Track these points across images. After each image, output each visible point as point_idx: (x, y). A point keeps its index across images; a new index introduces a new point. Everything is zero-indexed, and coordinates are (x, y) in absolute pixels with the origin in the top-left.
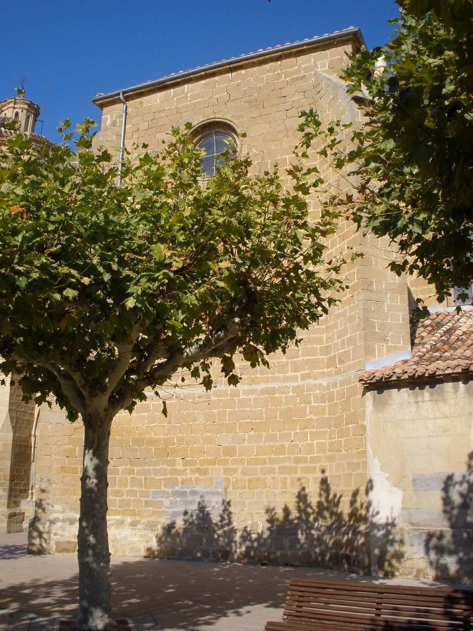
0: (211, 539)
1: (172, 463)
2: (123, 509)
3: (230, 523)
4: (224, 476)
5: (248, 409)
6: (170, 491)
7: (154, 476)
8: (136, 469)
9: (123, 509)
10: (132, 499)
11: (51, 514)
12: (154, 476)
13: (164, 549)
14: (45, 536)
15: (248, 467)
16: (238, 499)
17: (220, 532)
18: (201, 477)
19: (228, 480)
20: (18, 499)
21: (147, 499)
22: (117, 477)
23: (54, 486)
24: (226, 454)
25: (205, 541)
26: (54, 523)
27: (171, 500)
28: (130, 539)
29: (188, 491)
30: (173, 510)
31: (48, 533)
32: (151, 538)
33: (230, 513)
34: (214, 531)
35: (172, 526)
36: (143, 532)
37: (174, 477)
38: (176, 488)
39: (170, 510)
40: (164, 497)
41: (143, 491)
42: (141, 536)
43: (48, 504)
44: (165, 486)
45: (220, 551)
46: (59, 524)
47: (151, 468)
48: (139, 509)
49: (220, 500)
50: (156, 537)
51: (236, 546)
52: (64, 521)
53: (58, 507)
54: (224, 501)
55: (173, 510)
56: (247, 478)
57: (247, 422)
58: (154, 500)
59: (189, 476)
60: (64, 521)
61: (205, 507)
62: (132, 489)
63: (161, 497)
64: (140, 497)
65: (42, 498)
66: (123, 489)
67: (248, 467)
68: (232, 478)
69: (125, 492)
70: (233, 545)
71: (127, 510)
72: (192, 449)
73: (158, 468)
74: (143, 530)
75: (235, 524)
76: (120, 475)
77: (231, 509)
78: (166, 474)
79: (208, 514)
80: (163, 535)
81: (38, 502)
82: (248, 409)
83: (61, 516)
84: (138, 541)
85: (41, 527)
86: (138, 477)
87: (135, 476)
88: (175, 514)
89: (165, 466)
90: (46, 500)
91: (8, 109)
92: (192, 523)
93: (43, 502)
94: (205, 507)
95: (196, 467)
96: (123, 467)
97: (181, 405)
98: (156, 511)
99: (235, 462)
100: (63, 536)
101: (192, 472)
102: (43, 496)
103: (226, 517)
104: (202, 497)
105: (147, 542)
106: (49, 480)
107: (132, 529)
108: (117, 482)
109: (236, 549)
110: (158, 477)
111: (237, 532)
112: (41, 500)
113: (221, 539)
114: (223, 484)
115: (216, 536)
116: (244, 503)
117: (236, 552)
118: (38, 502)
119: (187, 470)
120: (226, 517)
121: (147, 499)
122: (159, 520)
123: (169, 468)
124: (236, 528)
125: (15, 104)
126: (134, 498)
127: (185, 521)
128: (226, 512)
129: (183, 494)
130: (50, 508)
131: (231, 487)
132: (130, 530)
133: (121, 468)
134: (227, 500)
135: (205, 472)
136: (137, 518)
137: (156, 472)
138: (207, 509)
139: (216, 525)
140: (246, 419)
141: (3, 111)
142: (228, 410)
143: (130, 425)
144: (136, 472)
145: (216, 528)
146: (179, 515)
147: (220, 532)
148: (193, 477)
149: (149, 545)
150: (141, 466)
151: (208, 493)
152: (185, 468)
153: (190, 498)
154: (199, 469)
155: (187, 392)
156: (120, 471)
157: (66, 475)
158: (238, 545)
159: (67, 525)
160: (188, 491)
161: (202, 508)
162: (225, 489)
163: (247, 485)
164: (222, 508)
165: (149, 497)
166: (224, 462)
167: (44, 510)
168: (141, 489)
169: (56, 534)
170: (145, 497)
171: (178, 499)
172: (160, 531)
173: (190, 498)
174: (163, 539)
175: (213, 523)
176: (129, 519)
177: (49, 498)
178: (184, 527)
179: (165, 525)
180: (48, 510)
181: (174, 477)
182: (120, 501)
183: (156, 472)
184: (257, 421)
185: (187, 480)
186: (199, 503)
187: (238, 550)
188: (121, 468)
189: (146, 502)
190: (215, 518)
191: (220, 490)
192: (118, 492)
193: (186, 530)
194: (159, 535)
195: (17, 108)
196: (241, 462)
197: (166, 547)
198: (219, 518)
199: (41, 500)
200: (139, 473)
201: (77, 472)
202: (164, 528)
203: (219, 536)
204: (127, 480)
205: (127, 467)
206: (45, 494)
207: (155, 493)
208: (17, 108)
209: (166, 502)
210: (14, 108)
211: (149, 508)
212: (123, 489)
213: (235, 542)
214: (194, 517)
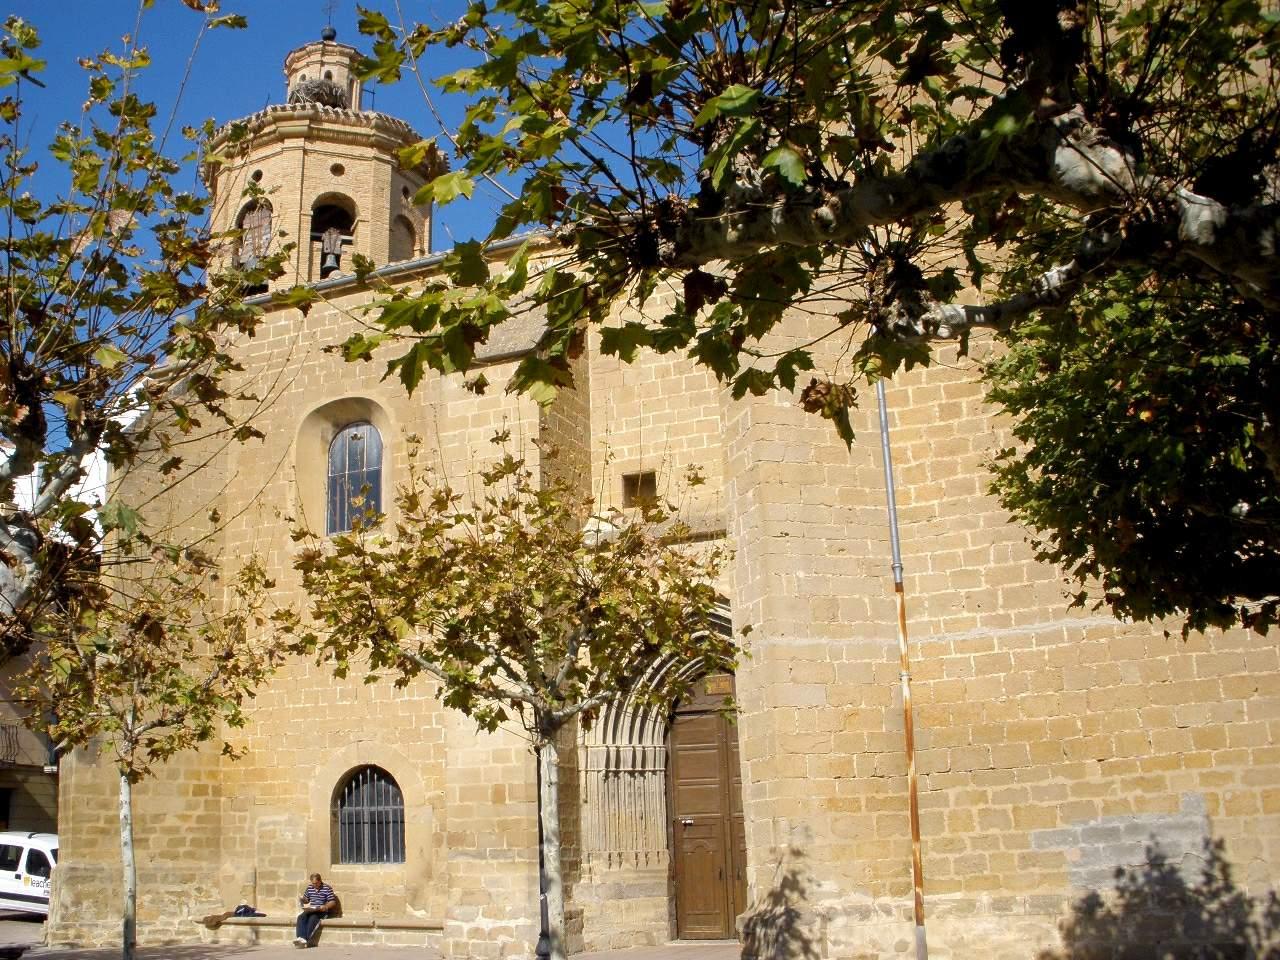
0: (1193, 923)
1: (1076, 771)
2: (968, 877)
3: (1228, 888)
4: (1202, 790)
5: (1240, 650)
6: (1079, 829)
7: (1036, 803)
8: (990, 790)
9: (968, 877)
10: (987, 854)
11: (818, 900)
12: (1036, 803)
13: (1083, 952)
14: (816, 947)
15: (1257, 767)
16: (1244, 835)
17: (1214, 906)
18: (1148, 796)
19: (1215, 798)
20: (569, 883)
21: (1024, 851)
22: (947, 811)
23: (818, 841)
24: (1200, 745)
25: (1179, 928)
26: (830, 920)
27: (1082, 849)
28: (995, 937)
29: (1122, 826)
30: (1090, 867)
31: (820, 940)
32: (1048, 932)
33: (1225, 868)
34: (1200, 907)
35: (1091, 904)
36: (1028, 921)
37: (1084, 799)
38: (1092, 823)
39: (1080, 870)
40: (1064, 842)
41: (1012, 836)
42: (1021, 930)
43: (810, 881)
44: (1065, 820)
45: (1219, 947)
46: (840, 921)
47: (1028, 785)
48: (1007, 873)
49: (1199, 840)
50: (1061, 927)
51: (1258, 934)
52: (847, 913)
53: (829, 886)
54: (1207, 843)
55: (1090, 867)
56: (1257, 790)
57: (1243, 677)
58: (1042, 851)
59: (1120, 795)
60: (847, 913)
61: (1164, 858)
62: (985, 833)
63: (1058, 844)
64: (1007, 847)
65: (797, 869)
66: (964, 835)
67: (1257, 767)
68: (1223, 792)
69: (968, 842)
70: (1250, 931)
71: (976, 878)
72: (1119, 739)
73: (1044, 783)
74: (1027, 918)
75: (1244, 886)
76: (952, 807)
77: (1228, 856)
78: (1065, 796)
79: (1173, 871)
80: (1078, 922)
81: (790, 877)
82: (1240, 650)
83: (837, 904)
84: (1016, 941)
85: (804, 930)
86: (997, 807)
87: (990, 805)
88: (1097, 877)
89: (1060, 780)
90: (804, 871)
91: (308, 65)
92: (1137, 893)
93: (799, 878)
94: (1164, 858)
95: (1135, 775)
96: (959, 789)
97: (1082, 652)
98: (1049, 874)
99: (1222, 760)
100: (851, 944)
101: (1126, 785)
102: (798, 864)
103: (1217, 873)
104: (1152, 836)
105: (1039, 939)
106: (807, 829)
107: (1000, 916)
108: (946, 823)
109: (1259, 939)
110: (1045, 804)
111: (1257, 903)
112: (794, 874)
113: (1218, 920)
114: (1202, 804)
115: (1205, 916)
116: (1258, 842)
117: (1259, 946)
118: (790, 877)
119: (1113, 782)
120: (1217, 873)
121: (1024, 851)
122: (1060, 891)
123: (1069, 782)
124: (1248, 895)
125: (323, 55)
126: (991, 852)
127: (1121, 891)
128: (1217, 865)
129: (1112, 833)
130: (815, 888)
131: (1222, 810)
132: (996, 919)
133: (952, 793)
134: (1216, 838)
135: (1157, 784)
136: (1006, 893)
137: (1040, 793)
138: (1167, 862)
139: (1198, 891)
140: (1237, 670)
141: (296, 70)
142: (1194, 655)
143: (964, 700)
144: (990, 797)
145: (1201, 899)
146: (1105, 878)
147: (1214, 906)
148: (1130, 796)
149: (1045, 946)
150: (1003, 784)
151: (1170, 827)
152: (1109, 779)
153: (1128, 841)
154: (1142, 778)
155: (1094, 623)
156: (952, 798)
157: (838, 815)
158: (1263, 933)
159: (855, 922)
160: (1122, 826)
161: (1155, 860)
162: (1207, 817)
163: (1259, 804)
164: (1206, 856)
165: (1028, 847)
166: (1201, 761)
167: (802, 893)
168: (1007, 832)
169: (836, 943)
170: (1017, 848)
171: (1101, 845)
172: (1068, 914)
173: (1128, 841)
174: (1078, 931)
175: (1190, 890)
176: (985, 898)
177: (810, 868)
178: (1121, 901)
179: (1077, 903)
180: (812, 893)
181: (1084, 799)
182: (956, 861)
183: (1040, 793)
184: (1265, 673)
185: (1116, 803)
186: (1149, 850)
187: (1266, 944)
188: (951, 793)
189: (1023, 857)
190: (1193, 880)
191: (1198, 819)
192: (951, 841)
193: (1129, 908)
194: (1066, 924)
195: (328, 63)
196: (1240, 758)
197: (1087, 948)
198: (1201, 879)
199: (794, 874)
200: (997, 798)
201: (860, 809)
202: (1077, 909)
203: (1213, 915)
204: (970, 817)
205: (968, 789)
206: (801, 859)
207: (1039, 837)
208: (328, 63)
209: (1072, 853)
210: (323, 64)
211: (1032, 869)
212: (964, 835)
213: (1255, 926)
214: (1141, 880)
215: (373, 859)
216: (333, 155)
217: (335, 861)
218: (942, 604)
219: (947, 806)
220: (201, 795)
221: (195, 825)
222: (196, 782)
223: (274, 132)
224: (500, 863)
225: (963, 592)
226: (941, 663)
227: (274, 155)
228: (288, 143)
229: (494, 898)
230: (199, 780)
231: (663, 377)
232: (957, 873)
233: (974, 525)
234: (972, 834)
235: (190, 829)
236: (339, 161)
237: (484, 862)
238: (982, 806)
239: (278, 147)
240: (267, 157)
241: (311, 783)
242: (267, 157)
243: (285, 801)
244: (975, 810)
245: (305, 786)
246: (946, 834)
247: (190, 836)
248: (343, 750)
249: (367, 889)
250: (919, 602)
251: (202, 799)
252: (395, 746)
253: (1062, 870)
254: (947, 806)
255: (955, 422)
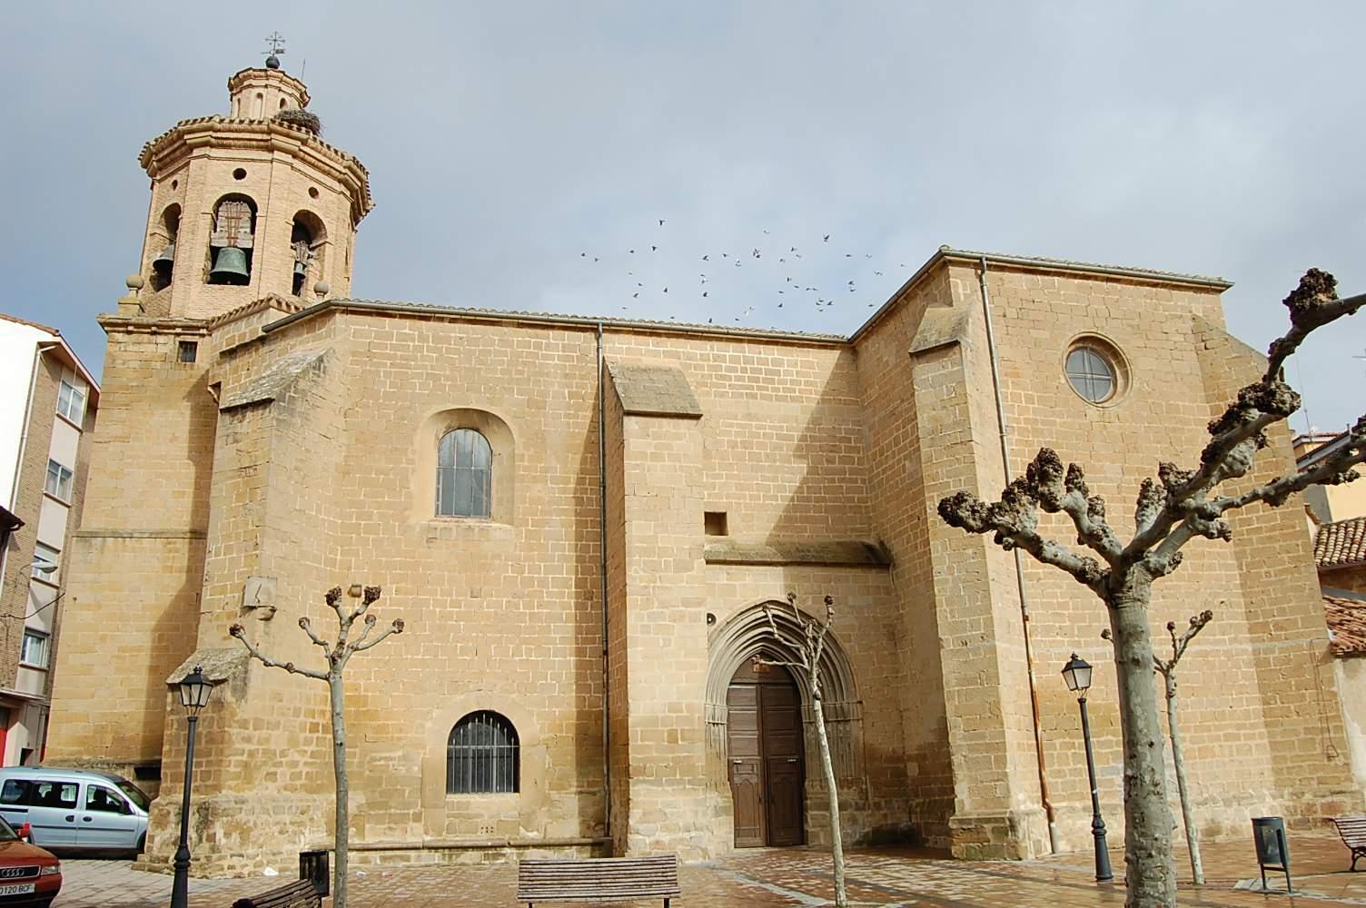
22: (1055, 753)
71: (1072, 794)
73: (1102, 739)
82: (1185, 672)
89: (1110, 737)
96: (1061, 740)
156: (1058, 746)
192: (1059, 771)
204: (1068, 756)
215: (473, 791)
216: (312, 178)
217: (449, 790)
218: (1047, 631)
219: (1055, 750)
220: (314, 732)
221: (310, 760)
222: (311, 720)
223: (267, 141)
224: (673, 790)
225: (1057, 625)
226: (1049, 665)
227: (261, 161)
228: (277, 155)
229: (669, 816)
230: (314, 718)
231: (733, 448)
232: (1063, 791)
233: (1061, 587)
234: (1070, 767)
235: (306, 763)
236: (316, 186)
237: (660, 789)
238: (1073, 751)
239: (266, 155)
240: (253, 160)
241: (429, 725)
242: (253, 160)
243: (399, 739)
244: (1070, 753)
245: (423, 726)
246: (1056, 767)
247: (305, 770)
248: (462, 697)
249: (482, 815)
250: (1036, 628)
251: (315, 735)
252: (514, 696)
253: (1113, 789)
254: (1055, 750)
255: (1049, 525)
